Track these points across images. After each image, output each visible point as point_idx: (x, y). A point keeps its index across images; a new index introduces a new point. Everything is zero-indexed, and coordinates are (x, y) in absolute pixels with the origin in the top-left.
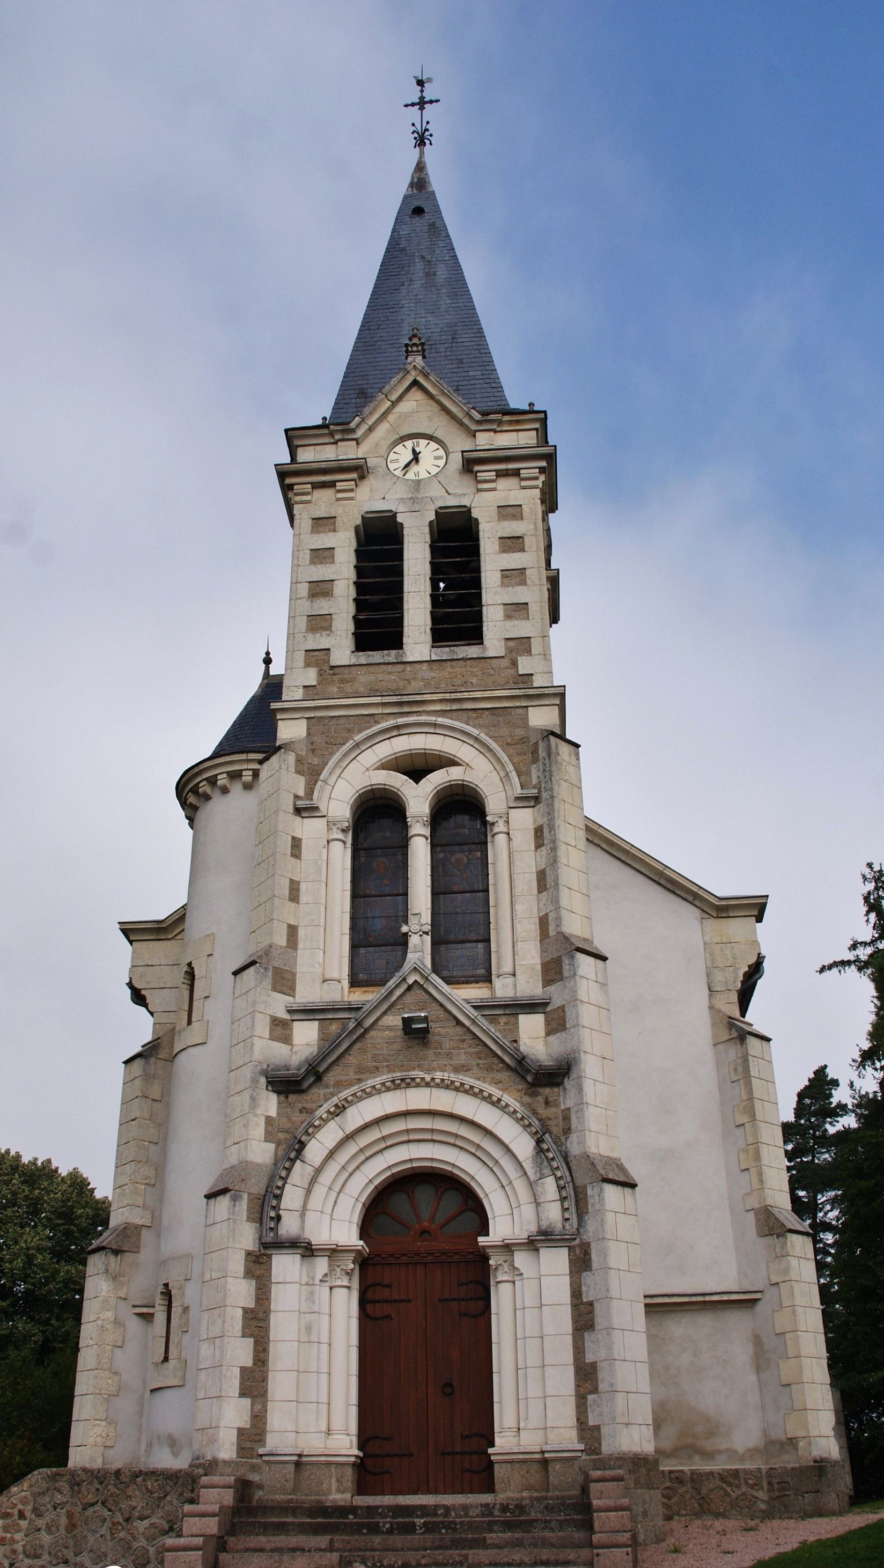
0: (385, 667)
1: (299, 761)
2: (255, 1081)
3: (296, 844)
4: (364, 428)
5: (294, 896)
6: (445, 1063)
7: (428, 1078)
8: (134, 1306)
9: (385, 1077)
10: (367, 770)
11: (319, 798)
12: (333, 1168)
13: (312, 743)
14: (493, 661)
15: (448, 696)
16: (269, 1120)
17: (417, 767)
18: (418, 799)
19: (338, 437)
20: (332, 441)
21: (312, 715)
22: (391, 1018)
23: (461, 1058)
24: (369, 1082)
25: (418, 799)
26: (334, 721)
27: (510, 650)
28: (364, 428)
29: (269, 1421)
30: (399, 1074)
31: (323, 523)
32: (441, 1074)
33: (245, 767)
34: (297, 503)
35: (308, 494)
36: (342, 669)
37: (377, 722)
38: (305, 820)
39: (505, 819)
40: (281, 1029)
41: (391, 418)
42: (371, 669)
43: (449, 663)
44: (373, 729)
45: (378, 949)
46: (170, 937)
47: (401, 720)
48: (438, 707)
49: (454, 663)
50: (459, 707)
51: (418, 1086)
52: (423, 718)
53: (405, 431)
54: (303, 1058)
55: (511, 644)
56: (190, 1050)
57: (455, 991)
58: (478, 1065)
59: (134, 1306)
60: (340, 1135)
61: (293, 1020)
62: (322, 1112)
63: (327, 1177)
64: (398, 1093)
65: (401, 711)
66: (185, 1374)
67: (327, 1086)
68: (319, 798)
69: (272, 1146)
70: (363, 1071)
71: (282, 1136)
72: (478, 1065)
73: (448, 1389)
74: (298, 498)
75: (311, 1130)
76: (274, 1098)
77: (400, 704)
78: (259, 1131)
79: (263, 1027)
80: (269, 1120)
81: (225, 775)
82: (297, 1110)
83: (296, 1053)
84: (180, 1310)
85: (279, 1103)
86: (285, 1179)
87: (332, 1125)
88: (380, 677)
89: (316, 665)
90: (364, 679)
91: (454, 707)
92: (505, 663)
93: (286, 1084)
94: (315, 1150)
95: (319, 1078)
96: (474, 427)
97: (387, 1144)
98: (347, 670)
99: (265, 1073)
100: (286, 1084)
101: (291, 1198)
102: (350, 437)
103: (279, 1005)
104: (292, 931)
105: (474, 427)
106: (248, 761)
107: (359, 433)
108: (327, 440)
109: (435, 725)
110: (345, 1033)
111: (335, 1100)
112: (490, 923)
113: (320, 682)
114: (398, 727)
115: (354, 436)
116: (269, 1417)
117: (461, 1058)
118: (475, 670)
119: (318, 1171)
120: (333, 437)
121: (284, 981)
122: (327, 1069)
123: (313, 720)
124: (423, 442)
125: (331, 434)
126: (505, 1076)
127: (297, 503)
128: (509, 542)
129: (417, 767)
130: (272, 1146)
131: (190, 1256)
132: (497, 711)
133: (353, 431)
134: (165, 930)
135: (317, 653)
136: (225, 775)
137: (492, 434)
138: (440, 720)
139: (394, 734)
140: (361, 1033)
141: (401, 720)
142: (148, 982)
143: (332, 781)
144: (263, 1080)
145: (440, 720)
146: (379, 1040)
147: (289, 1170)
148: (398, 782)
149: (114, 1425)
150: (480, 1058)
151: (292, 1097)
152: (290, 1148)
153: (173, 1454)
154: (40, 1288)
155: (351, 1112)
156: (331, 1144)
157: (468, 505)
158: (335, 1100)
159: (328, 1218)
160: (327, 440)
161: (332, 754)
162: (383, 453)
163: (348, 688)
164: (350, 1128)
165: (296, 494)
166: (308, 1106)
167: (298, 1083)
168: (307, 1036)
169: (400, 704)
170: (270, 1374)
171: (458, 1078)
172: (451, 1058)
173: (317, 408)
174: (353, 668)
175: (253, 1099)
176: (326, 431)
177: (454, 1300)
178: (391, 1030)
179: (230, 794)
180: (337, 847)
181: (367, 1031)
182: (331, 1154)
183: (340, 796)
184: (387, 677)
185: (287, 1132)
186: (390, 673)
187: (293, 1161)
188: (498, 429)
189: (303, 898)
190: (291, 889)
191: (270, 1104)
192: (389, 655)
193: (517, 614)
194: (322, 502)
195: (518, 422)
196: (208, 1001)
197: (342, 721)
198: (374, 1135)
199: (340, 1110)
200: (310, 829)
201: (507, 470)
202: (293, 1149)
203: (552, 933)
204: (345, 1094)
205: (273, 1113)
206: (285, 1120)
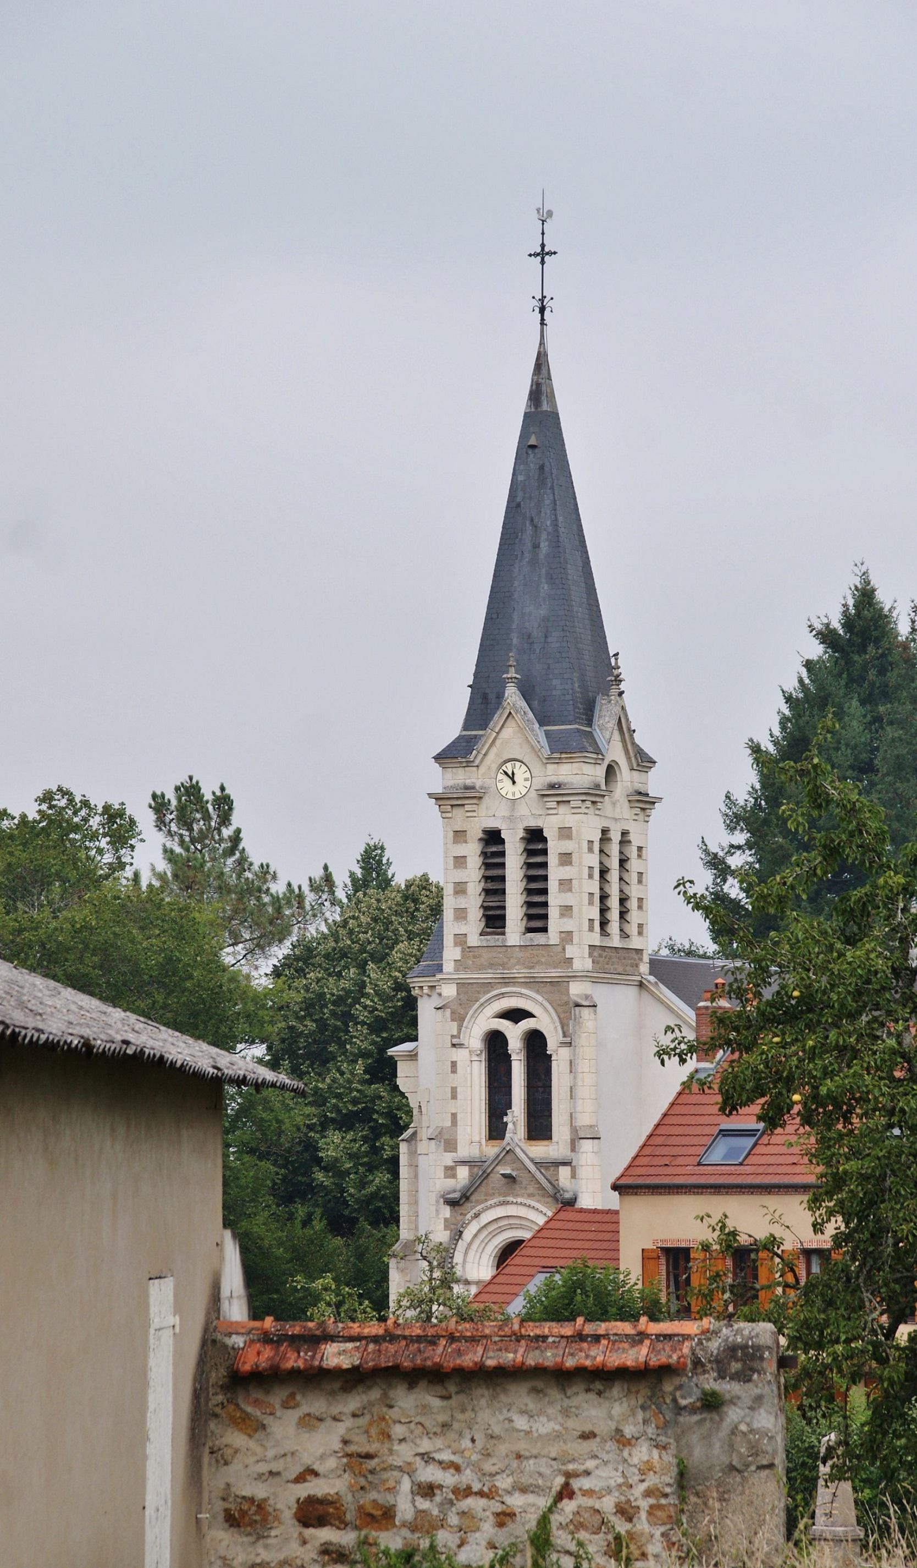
1: (452, 1013)
2: (437, 1202)
3: (454, 1064)
4: (480, 756)
5: (454, 1096)
11: (463, 1039)
12: (477, 1242)
16: (446, 1220)
17: (516, 1015)
25: (514, 1034)
27: (562, 940)
28: (480, 756)
31: (459, 835)
40: (450, 1172)
41: (498, 742)
47: (504, 990)
48: (523, 980)
52: (514, 989)
53: (505, 758)
55: (563, 935)
57: (534, 1148)
60: (478, 1227)
62: (468, 1217)
63: (474, 1247)
68: (464, 1037)
69: (448, 1232)
70: (489, 1195)
71: (453, 1227)
75: (465, 1225)
76: (448, 1208)
78: (441, 1226)
79: (441, 1173)
80: (446, 1220)
86: (455, 1249)
87: (474, 1222)
89: (461, 945)
90: (486, 956)
92: (560, 948)
93: (453, 1203)
94: (468, 1235)
95: (467, 1198)
97: (502, 1230)
99: (443, 1196)
101: (458, 1258)
103: (448, 1159)
104: (454, 1116)
110: (482, 1174)
111: (474, 1211)
113: (463, 957)
117: (531, 1189)
119: (470, 1244)
121: (450, 1145)
122: (471, 1194)
124: (518, 764)
126: (550, 1200)
129: (516, 1015)
130: (448, 1232)
137: (556, 766)
140: (486, 1176)
143: (470, 1026)
144: (442, 1200)
147: (456, 1244)
148: (505, 1026)
151: (457, 1208)
152: (455, 1234)
154: (812, 1059)
155: (482, 1216)
156: (474, 1232)
158: (474, 1211)
159: (476, 1265)
161: (471, 1007)
162: (493, 775)
164: (482, 1224)
167: (458, 1202)
168: (463, 1173)
171: (529, 1202)
173: (452, 727)
175: (437, 1211)
180: (476, 1064)
181: (489, 1174)
182: (476, 1236)
183: (475, 1039)
187: (458, 1240)
189: (459, 1097)
190: (452, 1092)
191: (446, 1211)
194: (459, 818)
198: (494, 1226)
199: (477, 1216)
200: (460, 1056)
202: (458, 1235)
203: (203, 1408)
204: (478, 1208)
205: (448, 1215)
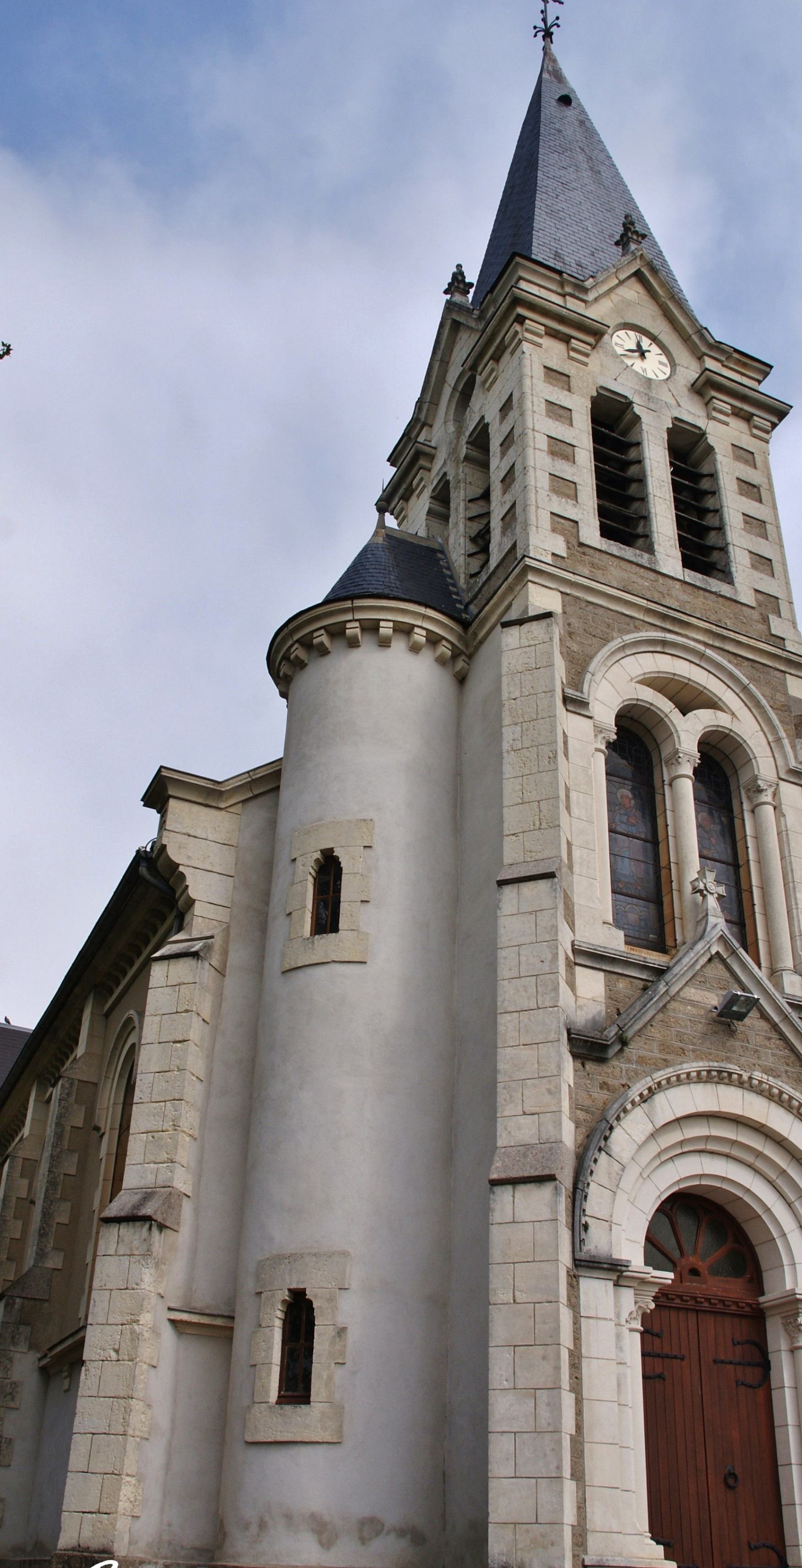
0: (638, 569)
6: (754, 1061)
7: (745, 1077)
8: (170, 1309)
9: (701, 1064)
10: (632, 680)
13: (569, 625)
14: (744, 608)
15: (714, 628)
18: (687, 732)
19: (568, 289)
20: (559, 291)
21: (569, 591)
22: (693, 990)
23: (770, 1062)
24: (685, 1066)
25: (687, 732)
26: (591, 607)
29: (588, 1516)
30: (716, 1064)
32: (760, 1074)
33: (419, 623)
34: (527, 340)
35: (540, 336)
36: (592, 551)
37: (637, 629)
38: (569, 714)
39: (773, 789)
42: (622, 563)
43: (701, 592)
44: (641, 634)
45: (629, 899)
46: (222, 805)
47: (670, 637)
49: (707, 594)
50: (722, 646)
51: (730, 1083)
54: (590, 1016)
55: (760, 597)
56: (332, 966)
58: (786, 1072)
59: (170, 1309)
61: (576, 964)
64: (710, 1087)
65: (663, 625)
66: (341, 1427)
67: (629, 1061)
72: (786, 1072)
73: (730, 1480)
74: (528, 336)
77: (664, 617)
81: (391, 624)
82: (597, 1084)
83: (581, 1007)
84: (331, 1331)
85: (575, 1071)
87: (638, 1114)
88: (634, 578)
91: (717, 644)
92: (755, 615)
93: (589, 1048)
96: (704, 349)
98: (597, 554)
100: (589, 1048)
102: (580, 296)
105: (704, 349)
106: (425, 617)
107: (591, 297)
108: (554, 287)
109: (702, 656)
112: (754, 905)
114: (664, 643)
115: (585, 298)
116: (588, 1510)
118: (728, 611)
120: (563, 287)
123: (568, 598)
125: (562, 284)
127: (527, 340)
128: (746, 486)
131: (345, 1254)
132: (756, 665)
133: (586, 290)
134: (219, 795)
135: (563, 521)
136: (391, 624)
138: (709, 652)
139: (659, 649)
141: (670, 637)
142: (189, 857)
145: (709, 652)
146: (681, 1016)
149: (752, 1546)
150: (787, 1065)
151: (589, 1066)
153: (321, 1544)
157: (703, 428)
160: (554, 287)
163: (599, 575)
165: (527, 330)
166: (610, 1081)
169: (664, 617)
170: (587, 1446)
172: (759, 1058)
174: (604, 555)
176: (557, 277)
177: (731, 1363)
178: (693, 1006)
179: (389, 650)
184: (640, 581)
185: (587, 1111)
186: (642, 577)
188: (726, 363)
192: (642, 556)
193: (761, 567)
195: (745, 365)
196: (368, 907)
197: (600, 611)
200: (572, 725)
201: (741, 409)
206: (584, 1095)
